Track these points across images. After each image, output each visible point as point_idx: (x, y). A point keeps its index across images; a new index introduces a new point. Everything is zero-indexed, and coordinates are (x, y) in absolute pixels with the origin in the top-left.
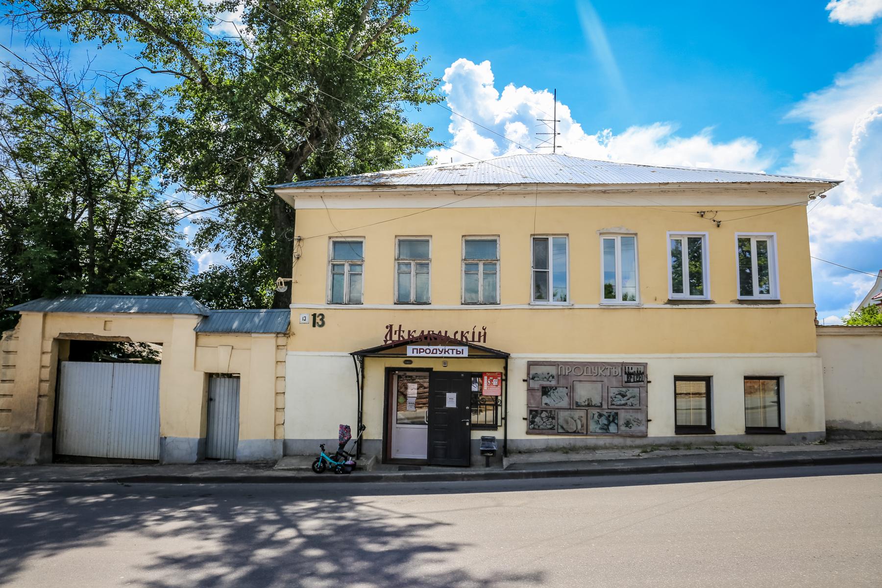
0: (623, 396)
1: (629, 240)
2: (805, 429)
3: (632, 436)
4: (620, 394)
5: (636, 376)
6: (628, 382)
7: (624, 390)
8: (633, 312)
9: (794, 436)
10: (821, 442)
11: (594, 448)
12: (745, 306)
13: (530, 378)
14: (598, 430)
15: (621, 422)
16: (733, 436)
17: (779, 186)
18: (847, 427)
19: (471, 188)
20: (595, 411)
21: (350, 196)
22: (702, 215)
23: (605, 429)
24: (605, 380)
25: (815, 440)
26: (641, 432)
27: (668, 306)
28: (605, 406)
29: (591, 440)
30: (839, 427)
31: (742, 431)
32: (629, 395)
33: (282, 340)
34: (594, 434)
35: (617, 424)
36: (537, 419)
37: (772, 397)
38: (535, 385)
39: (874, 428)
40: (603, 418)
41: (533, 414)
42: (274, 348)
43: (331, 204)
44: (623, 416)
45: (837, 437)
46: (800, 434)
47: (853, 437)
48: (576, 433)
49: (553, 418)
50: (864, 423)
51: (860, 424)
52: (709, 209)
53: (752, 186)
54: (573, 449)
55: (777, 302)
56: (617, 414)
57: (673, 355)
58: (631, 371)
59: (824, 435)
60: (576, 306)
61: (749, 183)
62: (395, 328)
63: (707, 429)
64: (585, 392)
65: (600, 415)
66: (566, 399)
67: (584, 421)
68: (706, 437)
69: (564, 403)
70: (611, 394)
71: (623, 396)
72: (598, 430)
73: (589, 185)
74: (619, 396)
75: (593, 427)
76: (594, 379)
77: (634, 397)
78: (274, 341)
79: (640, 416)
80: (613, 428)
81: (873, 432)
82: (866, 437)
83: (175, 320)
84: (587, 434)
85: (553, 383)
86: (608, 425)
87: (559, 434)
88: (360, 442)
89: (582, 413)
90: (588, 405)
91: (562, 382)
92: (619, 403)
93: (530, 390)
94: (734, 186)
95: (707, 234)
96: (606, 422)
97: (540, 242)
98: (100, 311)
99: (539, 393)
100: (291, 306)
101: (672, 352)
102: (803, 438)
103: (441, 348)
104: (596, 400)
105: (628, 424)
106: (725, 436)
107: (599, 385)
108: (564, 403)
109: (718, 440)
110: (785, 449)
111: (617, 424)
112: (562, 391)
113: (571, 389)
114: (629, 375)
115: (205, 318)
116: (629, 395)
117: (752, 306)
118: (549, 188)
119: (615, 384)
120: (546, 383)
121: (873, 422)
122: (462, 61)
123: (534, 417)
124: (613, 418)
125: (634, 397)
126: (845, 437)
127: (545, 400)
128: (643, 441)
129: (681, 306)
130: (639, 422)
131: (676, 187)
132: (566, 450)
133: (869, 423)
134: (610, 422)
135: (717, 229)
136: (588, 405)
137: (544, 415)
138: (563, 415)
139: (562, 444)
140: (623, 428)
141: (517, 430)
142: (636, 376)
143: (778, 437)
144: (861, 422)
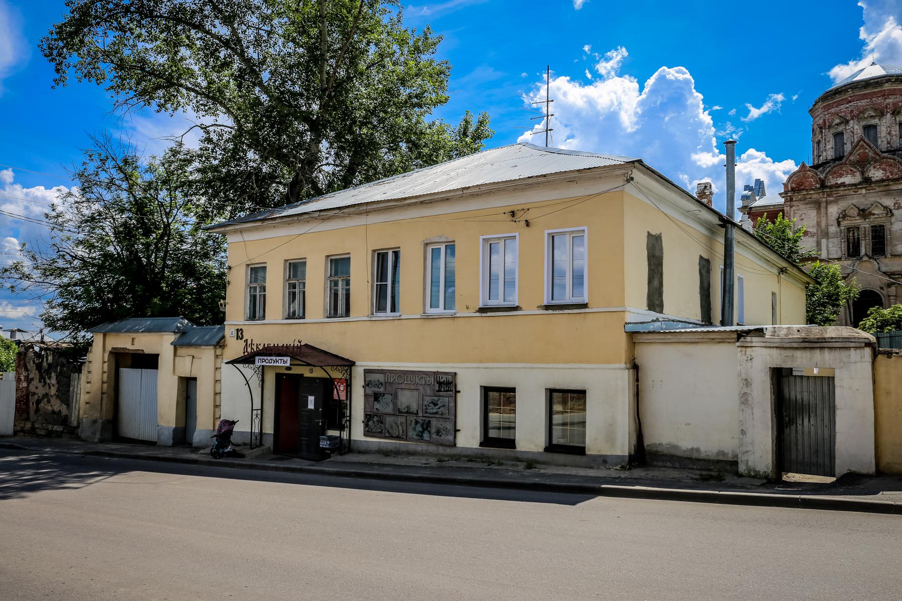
0: (435, 405)
1: (451, 248)
2: (607, 451)
3: (442, 445)
4: (432, 403)
5: (446, 385)
6: (439, 391)
7: (436, 398)
8: (450, 321)
9: (595, 458)
10: (623, 468)
11: (410, 453)
12: (550, 312)
13: (367, 384)
14: (415, 437)
15: (433, 430)
16: (533, 453)
17: (577, 174)
18: (673, 452)
19: (322, 213)
20: (413, 418)
21: (256, 229)
22: (513, 214)
23: (420, 435)
24: (421, 388)
25: (616, 465)
26: (449, 441)
27: (478, 314)
28: (420, 414)
29: (412, 446)
30: (665, 452)
31: (541, 450)
32: (440, 404)
33: (219, 351)
34: (412, 440)
35: (429, 432)
36: (370, 423)
37: (493, 416)
38: (370, 391)
39: (703, 456)
40: (419, 425)
41: (368, 417)
42: (213, 357)
43: (248, 237)
44: (435, 423)
45: (660, 464)
46: (601, 456)
47: (677, 465)
48: (398, 438)
49: (382, 423)
50: (692, 449)
51: (688, 450)
52: (520, 207)
53: (549, 178)
54: (397, 453)
55: (516, 308)
56: (429, 422)
57: (482, 365)
58: (442, 380)
59: (627, 459)
60: (458, 315)
61: (545, 176)
62: (249, 342)
63: (455, 445)
64: (408, 399)
65: (417, 422)
66: (391, 405)
67: (405, 427)
68: (507, 452)
69: (389, 409)
70: (425, 403)
71: (435, 405)
72: (415, 437)
73: (405, 199)
74: (432, 405)
75: (411, 433)
76: (413, 387)
77: (444, 406)
78: (213, 351)
79: (449, 426)
80: (426, 436)
81: (698, 460)
82: (690, 466)
83: (165, 337)
84: (406, 440)
85: (382, 390)
86: (422, 432)
87: (385, 438)
88: (261, 433)
89: (401, 419)
90: (407, 412)
91: (389, 389)
92: (431, 411)
93: (366, 395)
94: (530, 181)
95: (547, 232)
96: (421, 429)
97: (381, 257)
98: (128, 331)
99: (372, 399)
100: (225, 323)
101: (481, 362)
102: (603, 461)
103: (274, 358)
104: (414, 407)
105: (438, 432)
106: (525, 452)
107: (415, 393)
108: (389, 409)
109: (519, 456)
110: (582, 472)
111: (429, 432)
112: (388, 398)
113: (395, 396)
114: (440, 384)
115: (183, 333)
116: (440, 404)
117: (557, 312)
118: (375, 206)
119: (429, 392)
120: (376, 390)
121: (702, 449)
122: (664, 68)
123: (368, 421)
124: (426, 426)
125: (444, 406)
126: (668, 464)
127: (377, 406)
128: (449, 451)
129: (489, 314)
130: (447, 432)
131: (477, 190)
132: (386, 453)
133: (698, 450)
134: (424, 430)
135: (527, 229)
136: (407, 412)
137: (375, 419)
138: (389, 420)
139: (390, 448)
140: (434, 436)
141: (358, 433)
142: (446, 385)
143: (578, 458)
144: (689, 447)
